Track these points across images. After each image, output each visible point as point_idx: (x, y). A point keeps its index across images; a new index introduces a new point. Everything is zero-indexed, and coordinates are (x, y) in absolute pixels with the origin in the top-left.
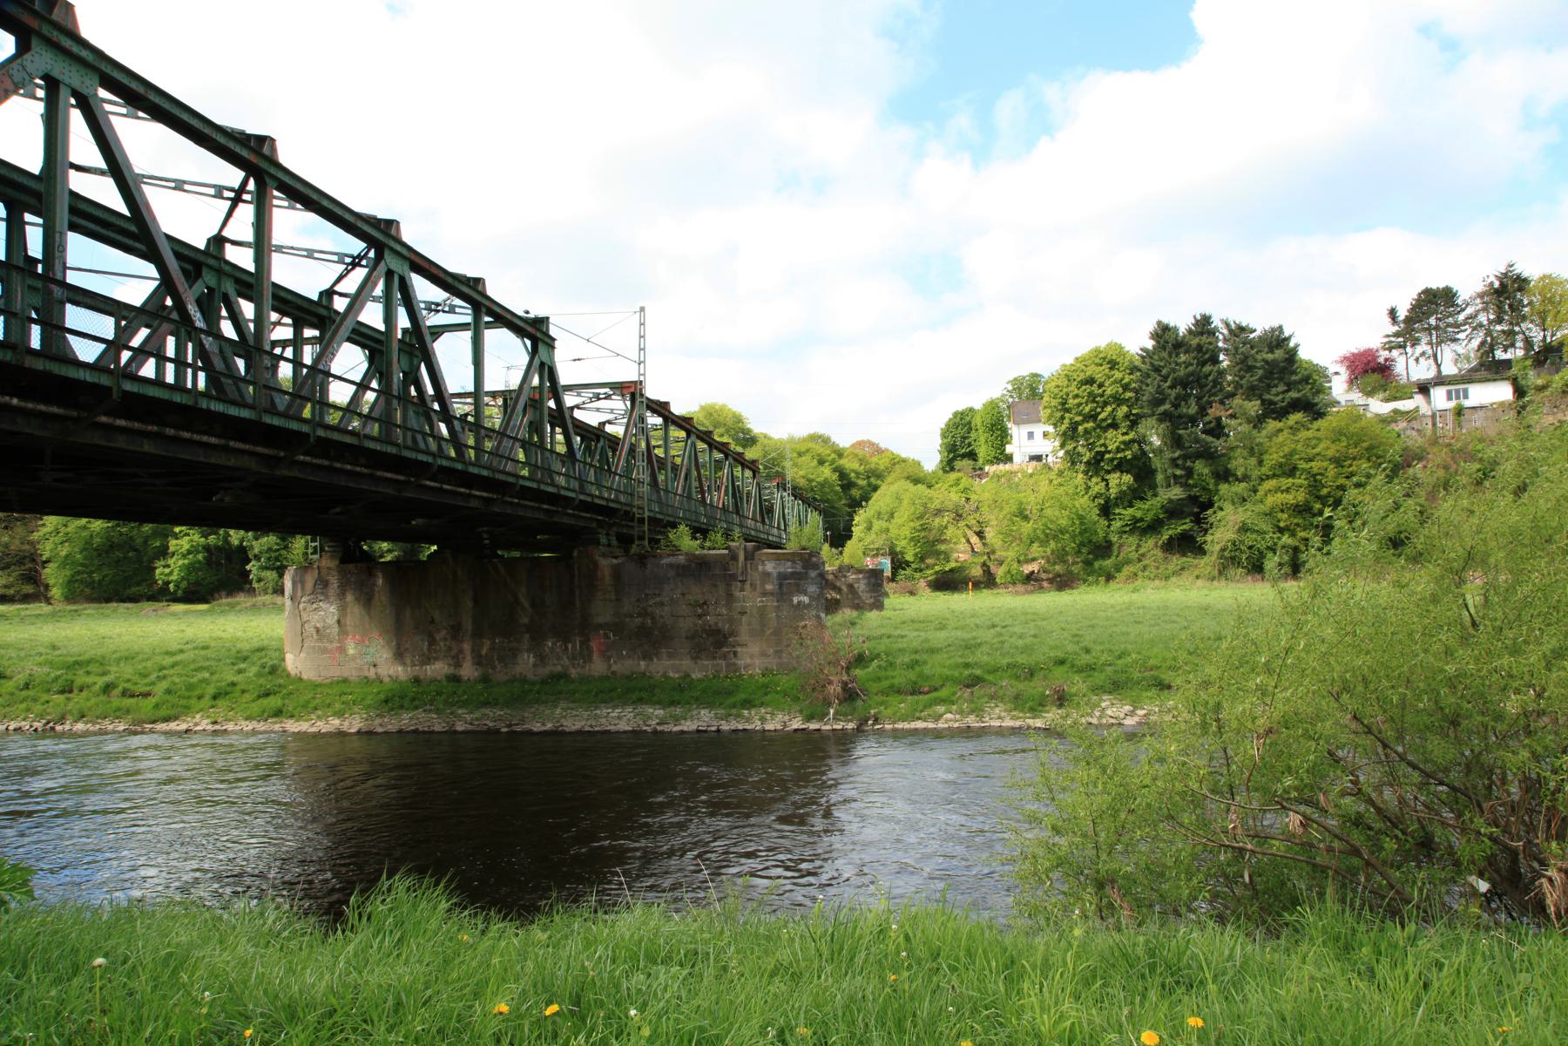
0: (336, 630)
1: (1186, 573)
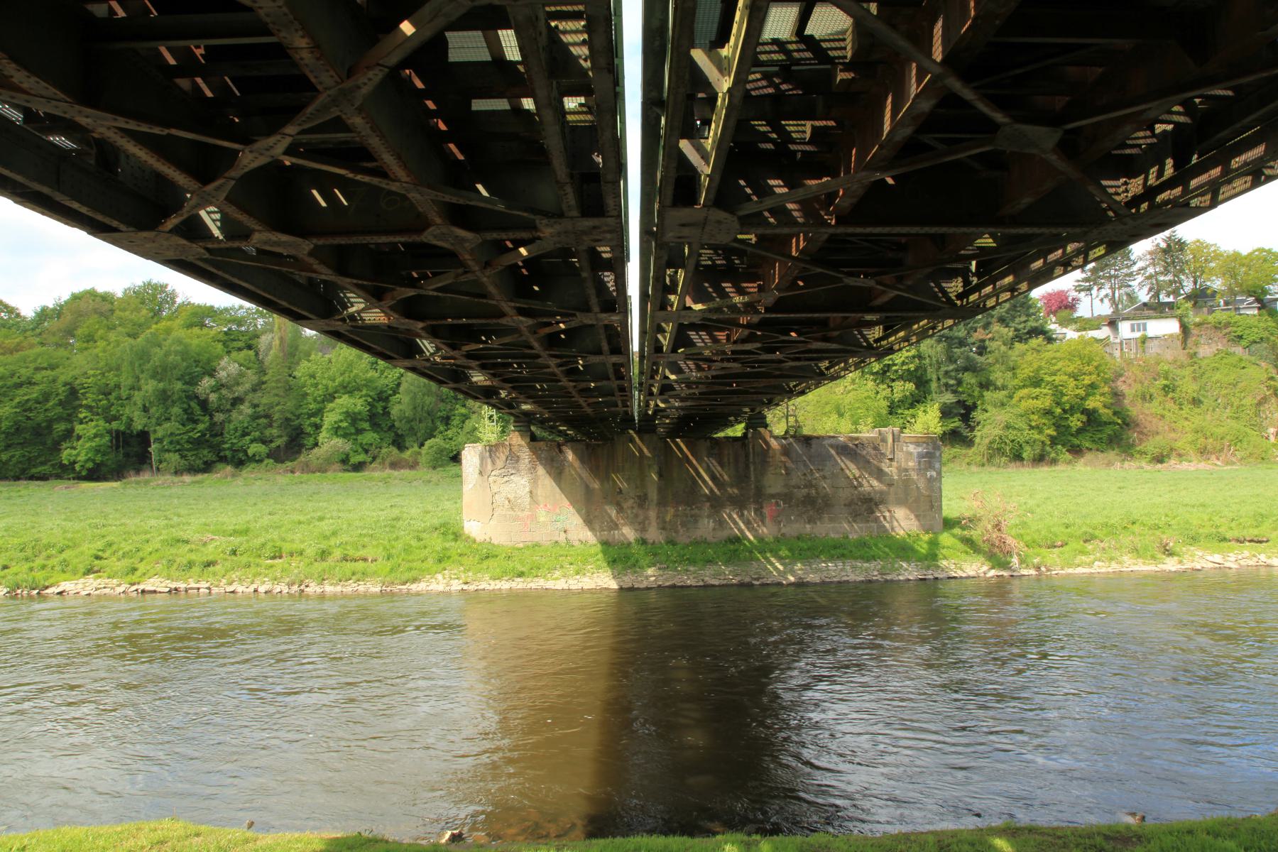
0: (528, 499)
1: (957, 460)
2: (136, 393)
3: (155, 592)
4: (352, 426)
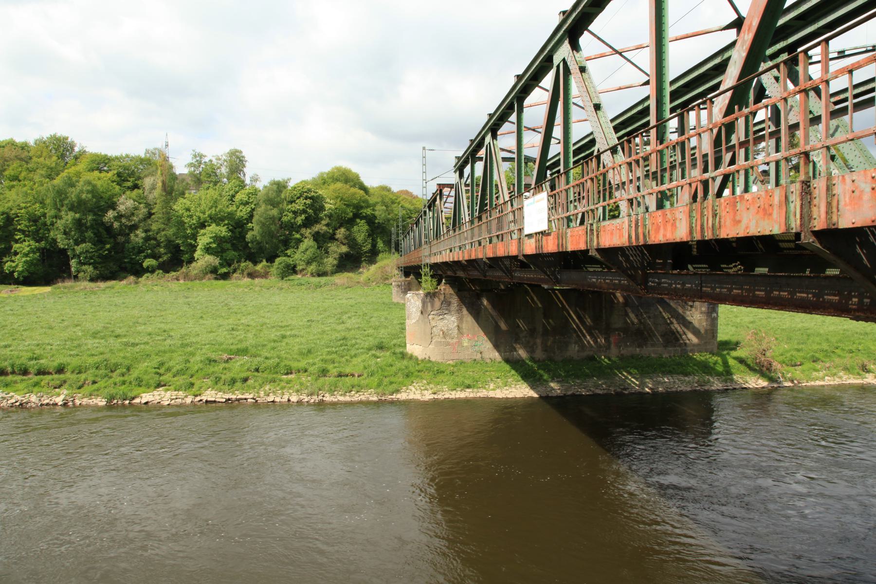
2: (59, 221)
3: (215, 401)
4: (218, 248)
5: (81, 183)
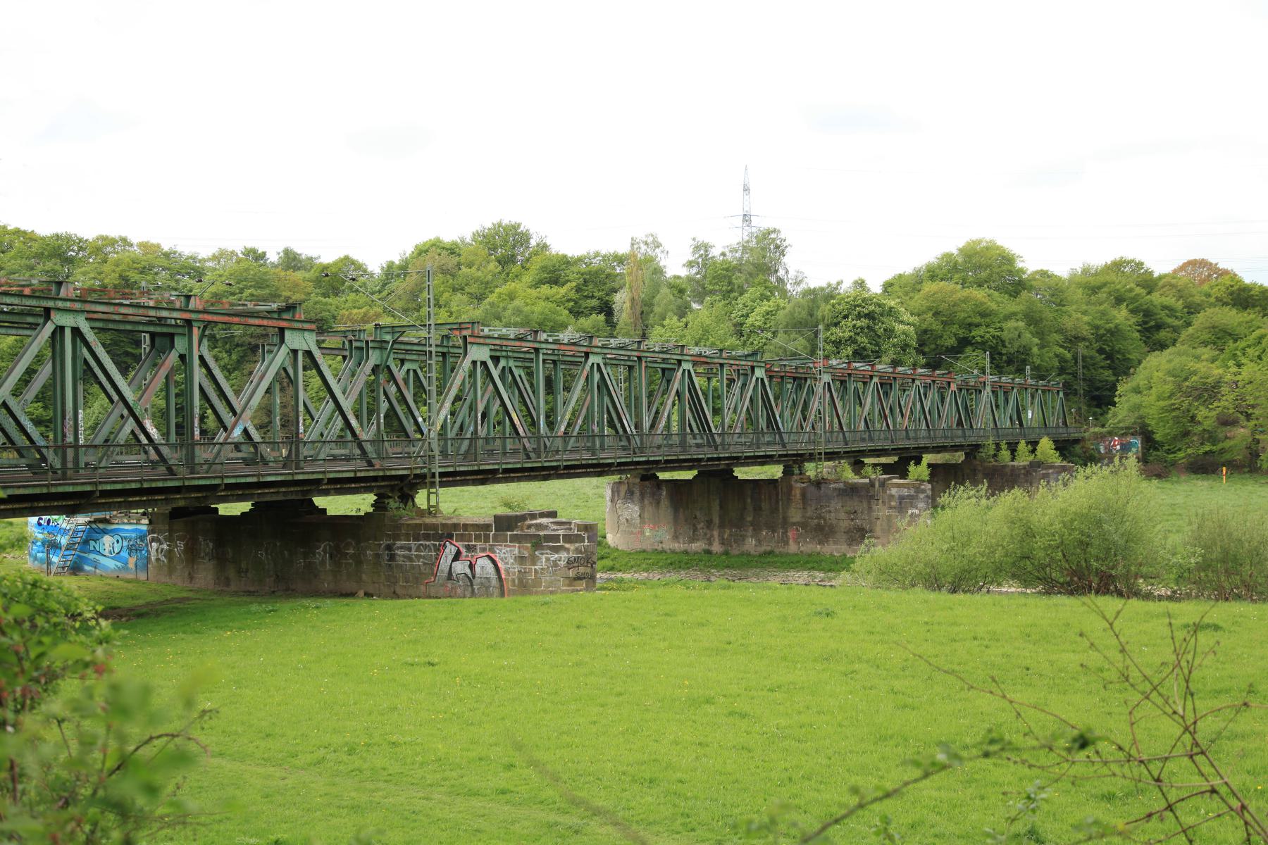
0: (638, 521)
5: (509, 312)
